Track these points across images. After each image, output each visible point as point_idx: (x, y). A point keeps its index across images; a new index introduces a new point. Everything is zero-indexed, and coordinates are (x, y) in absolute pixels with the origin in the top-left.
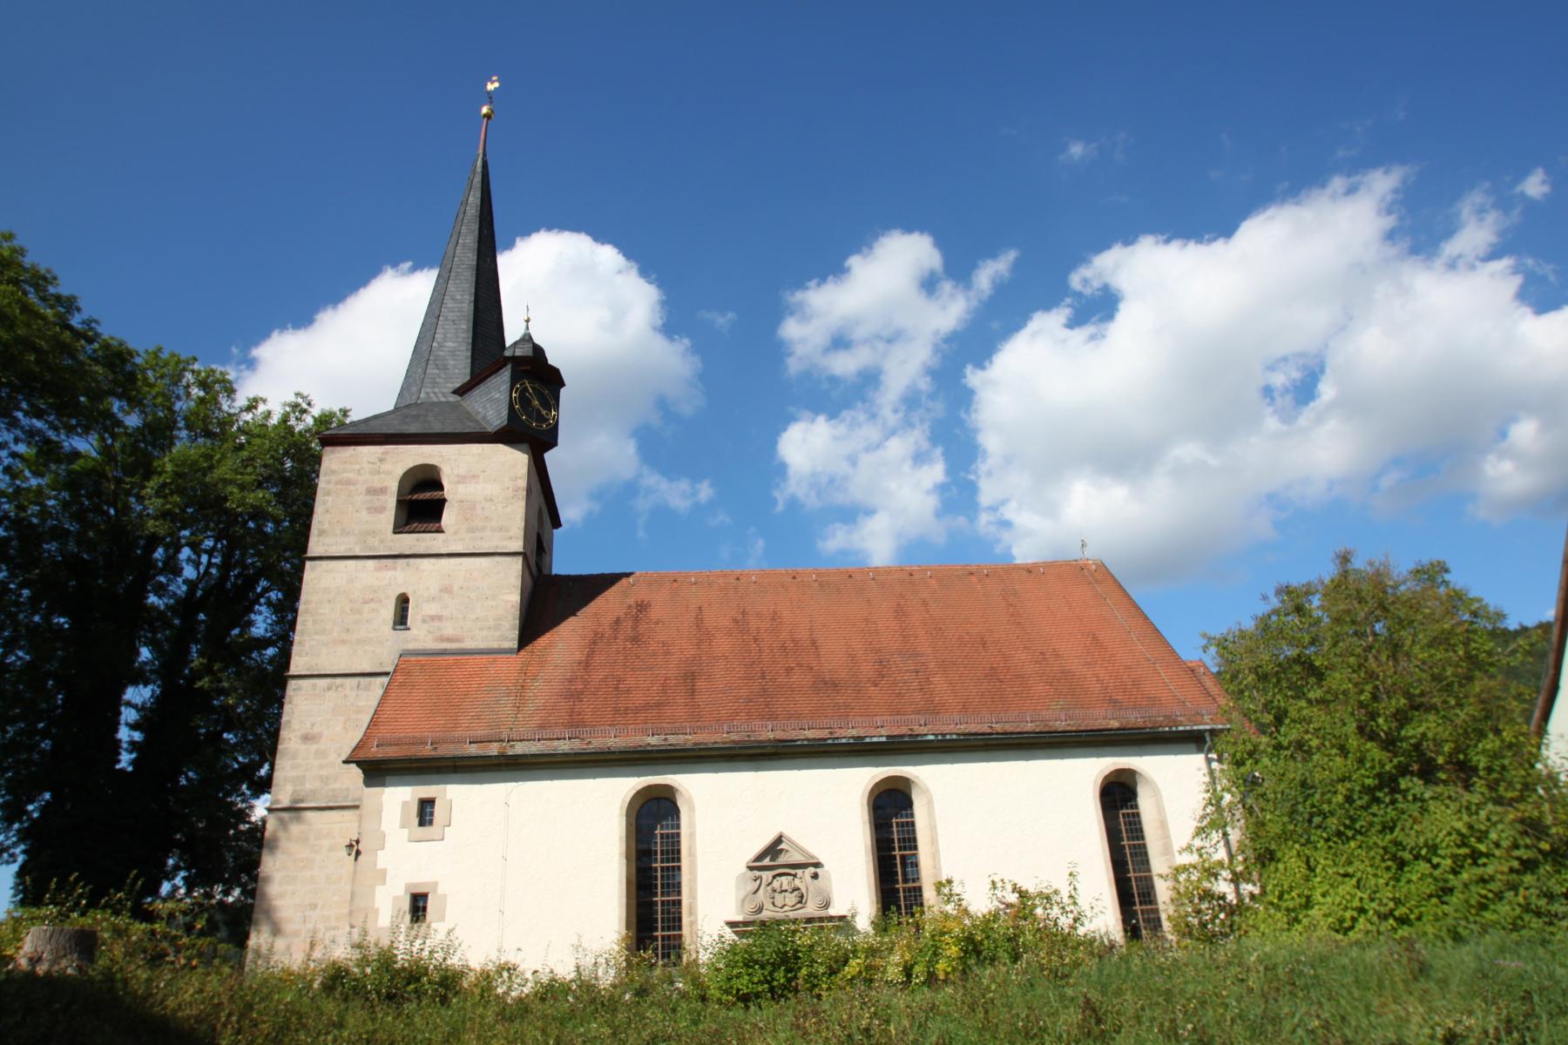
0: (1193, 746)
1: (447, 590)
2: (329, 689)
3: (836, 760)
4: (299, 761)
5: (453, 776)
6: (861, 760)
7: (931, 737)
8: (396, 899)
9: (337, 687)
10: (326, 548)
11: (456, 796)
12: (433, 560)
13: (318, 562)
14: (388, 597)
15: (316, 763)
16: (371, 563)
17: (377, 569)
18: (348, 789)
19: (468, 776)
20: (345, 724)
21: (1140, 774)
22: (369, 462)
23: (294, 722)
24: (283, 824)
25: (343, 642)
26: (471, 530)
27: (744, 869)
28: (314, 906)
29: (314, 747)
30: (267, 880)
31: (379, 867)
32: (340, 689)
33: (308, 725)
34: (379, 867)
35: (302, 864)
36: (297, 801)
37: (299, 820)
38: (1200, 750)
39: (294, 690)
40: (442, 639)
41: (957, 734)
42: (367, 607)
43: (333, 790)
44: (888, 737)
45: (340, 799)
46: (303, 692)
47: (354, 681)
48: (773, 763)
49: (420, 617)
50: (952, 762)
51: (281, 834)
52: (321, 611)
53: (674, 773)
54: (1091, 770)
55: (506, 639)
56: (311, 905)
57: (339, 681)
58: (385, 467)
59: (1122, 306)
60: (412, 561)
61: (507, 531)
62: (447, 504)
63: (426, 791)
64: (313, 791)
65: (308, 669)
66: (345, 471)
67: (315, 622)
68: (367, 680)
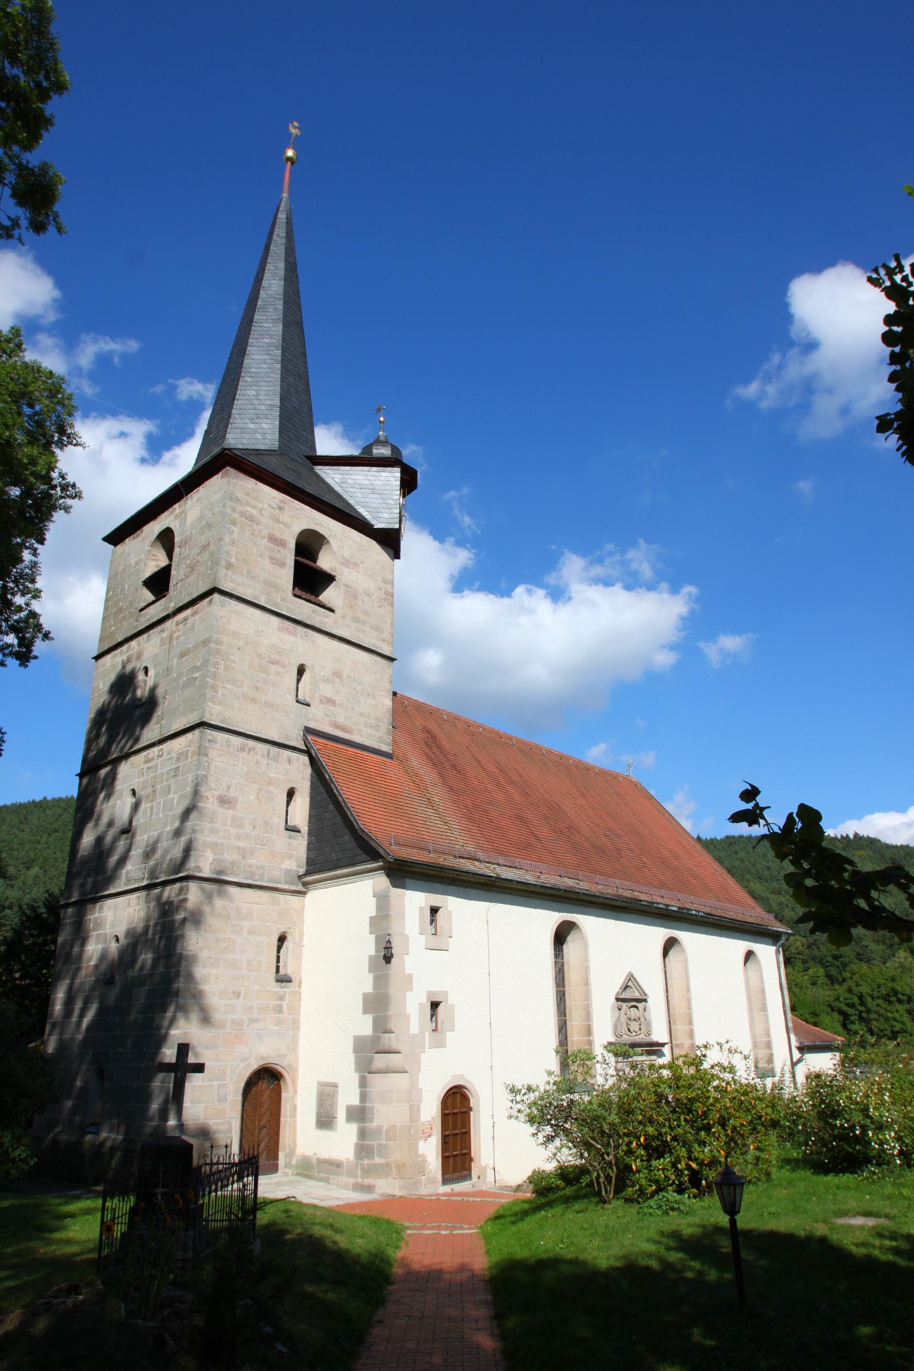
0: (770, 940)
1: (337, 674)
2: (243, 750)
3: (507, 897)
4: (217, 825)
5: (452, 888)
6: (554, 904)
7: (694, 912)
8: (421, 1005)
9: (250, 750)
10: (233, 585)
11: (689, 939)
12: (326, 639)
13: (227, 599)
14: (290, 664)
15: (233, 831)
16: (275, 620)
17: (280, 629)
18: (263, 867)
19: (460, 889)
20: (258, 793)
21: (755, 955)
22: (270, 505)
23: (210, 779)
24: (209, 897)
25: (254, 700)
26: (356, 620)
27: (614, 1000)
28: (237, 995)
29: (231, 813)
30: (194, 959)
31: (406, 972)
32: (252, 753)
33: (225, 787)
34: (406, 972)
35: (224, 945)
36: (221, 872)
37: (221, 894)
38: (774, 944)
39: (209, 741)
40: (336, 726)
41: (704, 913)
42: (274, 668)
43: (250, 866)
44: (679, 908)
45: (257, 877)
46: (218, 746)
47: (266, 747)
48: (590, 910)
49: (317, 695)
50: (598, 916)
51: (207, 909)
52: (232, 657)
53: (578, 913)
54: (550, 919)
55: (383, 742)
56: (234, 992)
57: (251, 743)
58: (284, 517)
59: (436, 544)
60: (309, 632)
61: (381, 632)
62: (334, 584)
63: (436, 899)
64: (233, 863)
65: (221, 721)
66: (249, 505)
67: (226, 668)
68: (276, 750)
